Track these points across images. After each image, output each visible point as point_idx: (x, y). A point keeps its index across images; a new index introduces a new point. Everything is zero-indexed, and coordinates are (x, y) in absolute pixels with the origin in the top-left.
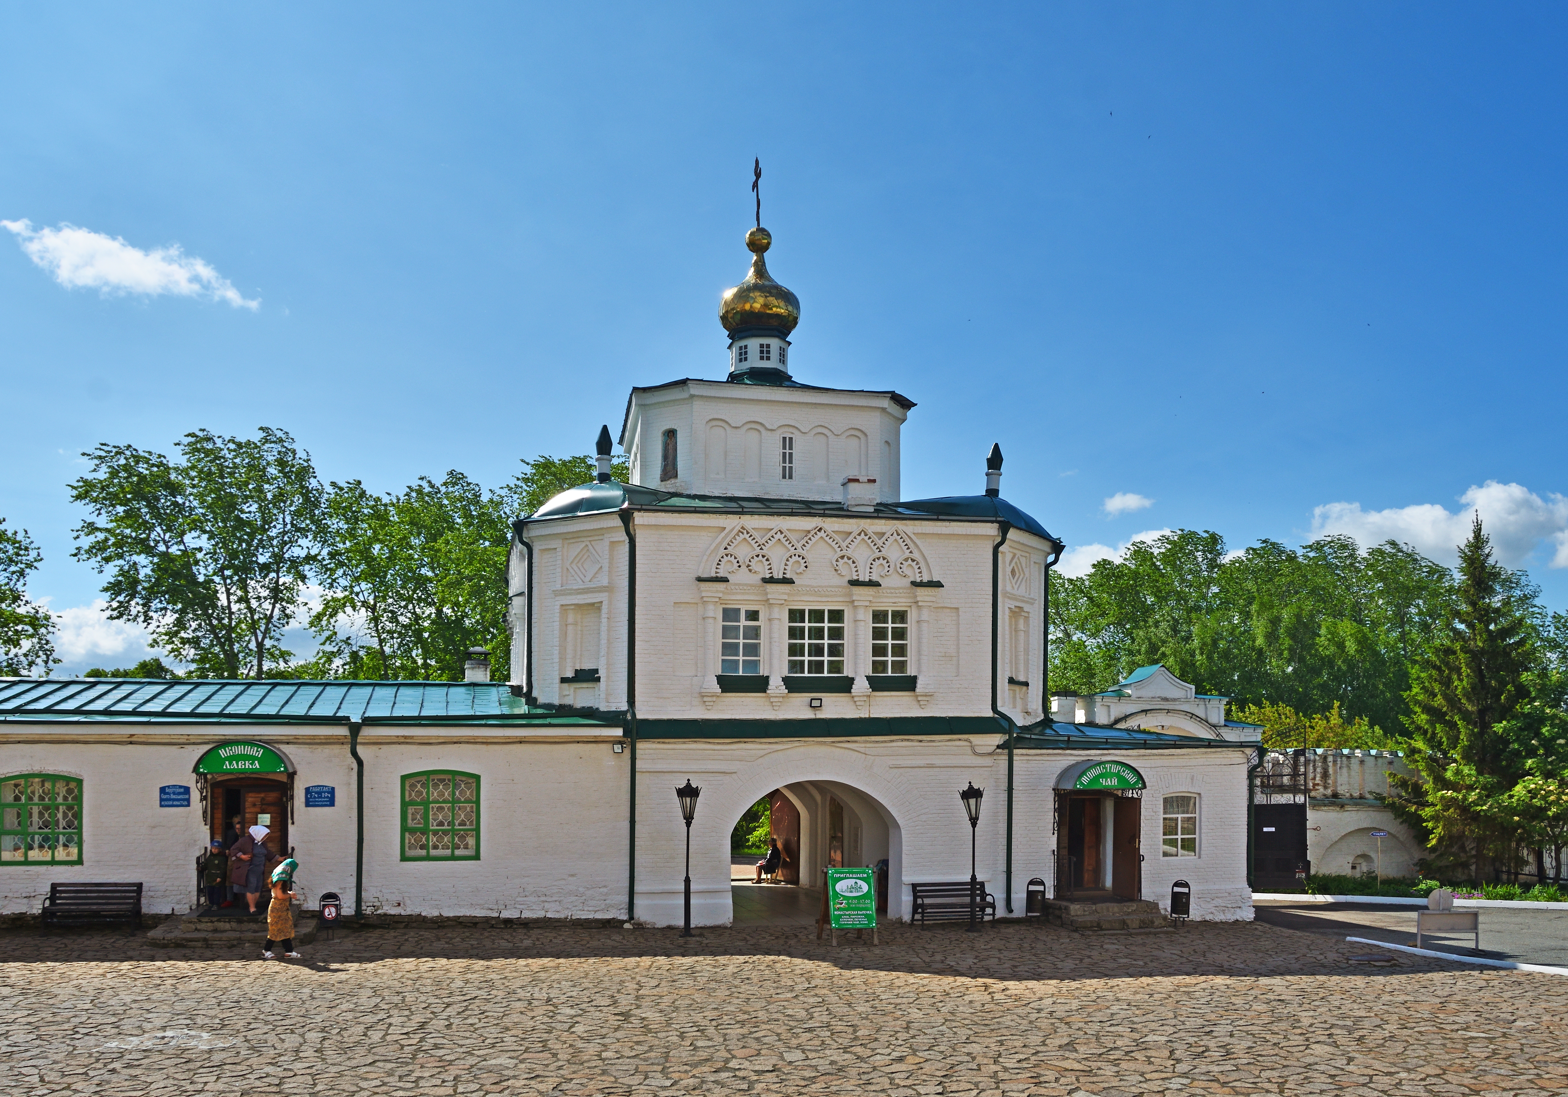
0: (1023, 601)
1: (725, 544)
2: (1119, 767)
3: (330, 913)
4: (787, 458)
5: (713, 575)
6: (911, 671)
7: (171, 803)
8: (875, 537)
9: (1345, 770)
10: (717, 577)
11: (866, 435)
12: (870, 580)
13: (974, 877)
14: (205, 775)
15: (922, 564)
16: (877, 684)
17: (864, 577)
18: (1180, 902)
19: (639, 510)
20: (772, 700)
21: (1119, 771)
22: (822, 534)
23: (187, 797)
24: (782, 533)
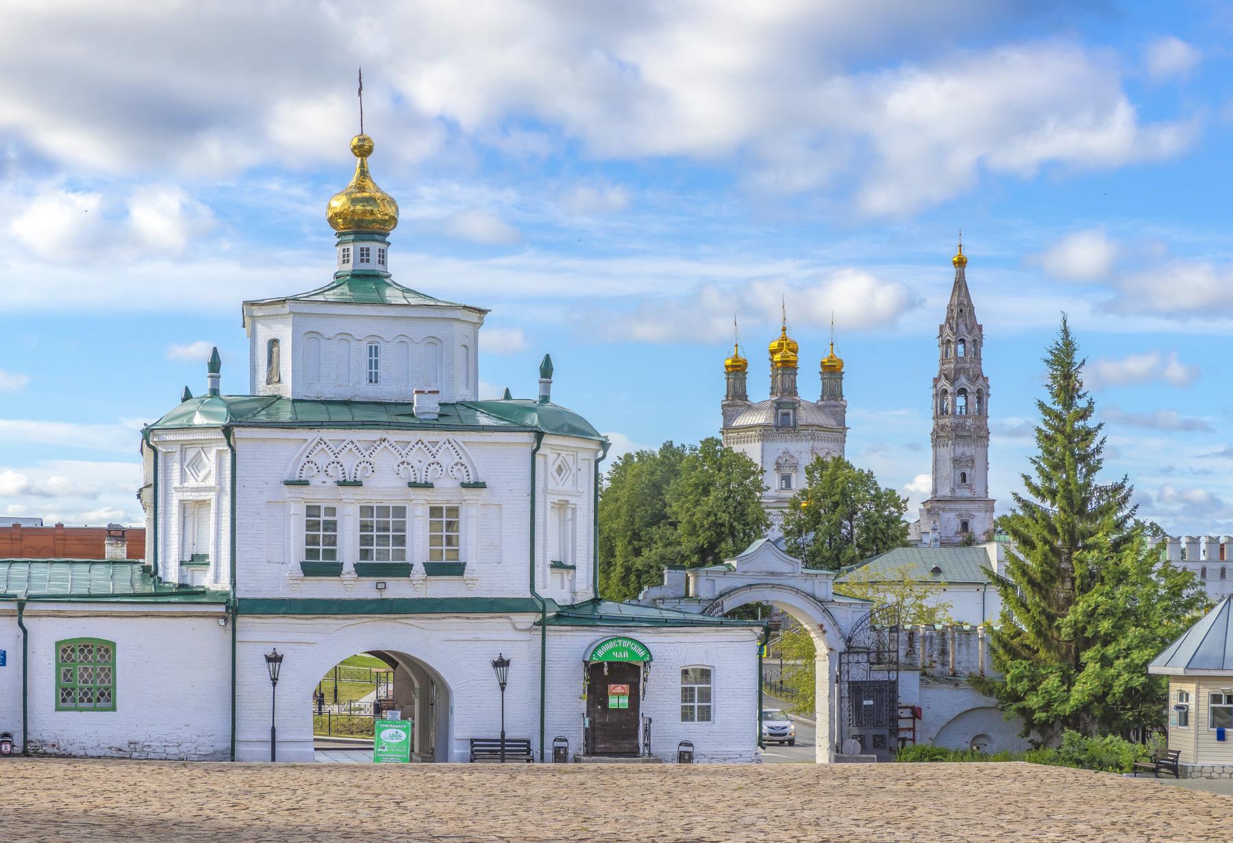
0: (568, 495)
1: (307, 453)
2: (629, 643)
4: (374, 364)
5: (297, 478)
8: (429, 446)
9: (964, 648)
10: (300, 481)
11: (441, 342)
12: (426, 482)
13: (503, 734)
15: (469, 468)
16: (434, 569)
17: (421, 479)
19: (238, 426)
21: (629, 646)
22: (386, 444)
24: (353, 443)
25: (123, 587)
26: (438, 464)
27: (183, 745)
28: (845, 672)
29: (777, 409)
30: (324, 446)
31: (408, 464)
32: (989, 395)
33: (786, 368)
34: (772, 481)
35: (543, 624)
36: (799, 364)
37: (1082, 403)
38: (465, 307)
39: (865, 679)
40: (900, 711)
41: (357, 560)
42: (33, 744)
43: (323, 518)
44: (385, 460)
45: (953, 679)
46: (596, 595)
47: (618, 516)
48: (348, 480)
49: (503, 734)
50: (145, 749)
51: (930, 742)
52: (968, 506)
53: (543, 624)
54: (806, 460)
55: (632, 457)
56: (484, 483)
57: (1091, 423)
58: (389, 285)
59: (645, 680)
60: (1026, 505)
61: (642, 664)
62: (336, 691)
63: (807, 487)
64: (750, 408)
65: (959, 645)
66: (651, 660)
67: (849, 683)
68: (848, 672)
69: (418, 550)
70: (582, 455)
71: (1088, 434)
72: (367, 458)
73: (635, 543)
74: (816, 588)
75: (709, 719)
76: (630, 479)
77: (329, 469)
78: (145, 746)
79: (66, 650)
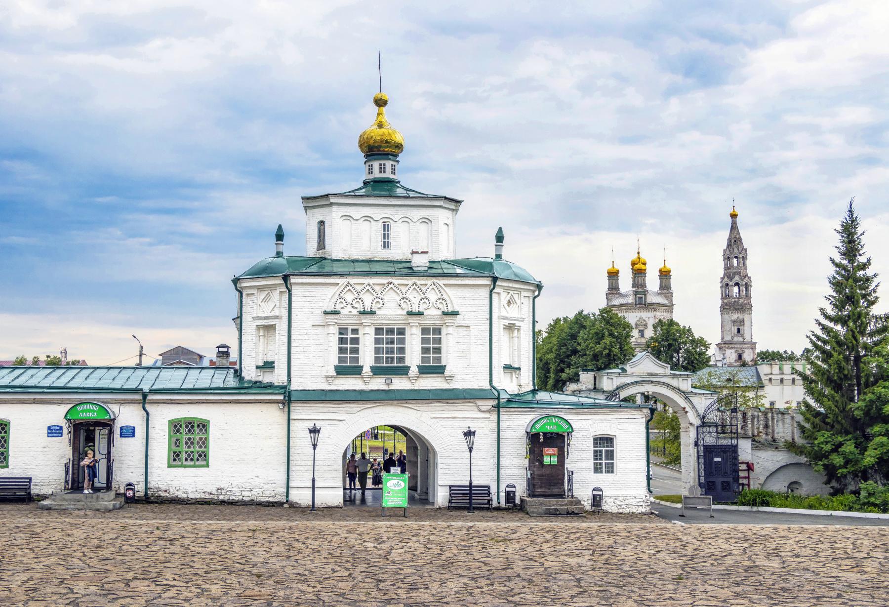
0: (515, 320)
1: (339, 292)
3: (130, 494)
6: (443, 363)
7: (53, 435)
9: (780, 424)
11: (431, 222)
12: (419, 311)
13: (471, 483)
14: (70, 420)
15: (448, 302)
16: (424, 370)
18: (597, 500)
19: (293, 275)
20: (365, 379)
22: (391, 286)
23: (61, 431)
24: (369, 285)
25: (218, 382)
26: (427, 299)
27: (254, 490)
28: (701, 439)
29: (636, 295)
30: (351, 288)
31: (407, 299)
32: (751, 286)
33: (639, 273)
34: (635, 333)
35: (498, 407)
36: (647, 271)
37: (862, 260)
38: (446, 198)
39: (715, 444)
40: (740, 465)
41: (373, 363)
42: (151, 490)
43: (350, 335)
44: (391, 298)
45: (773, 444)
46: (534, 387)
47: (551, 351)
48: (366, 310)
49: (471, 483)
50: (228, 493)
51: (760, 487)
52: (741, 346)
53: (498, 407)
54: (651, 322)
55: (560, 320)
56: (458, 312)
57: (869, 272)
58: (398, 187)
59: (568, 445)
60: (824, 328)
61: (567, 434)
62: (394, 447)
63: (653, 335)
64: (621, 295)
65: (777, 421)
66: (573, 431)
67: (704, 446)
68: (703, 439)
69: (414, 357)
70: (524, 294)
71: (868, 280)
72: (380, 295)
73: (561, 365)
74: (680, 384)
75: (612, 472)
76: (557, 333)
77: (354, 303)
78: (228, 491)
79: (175, 426)
